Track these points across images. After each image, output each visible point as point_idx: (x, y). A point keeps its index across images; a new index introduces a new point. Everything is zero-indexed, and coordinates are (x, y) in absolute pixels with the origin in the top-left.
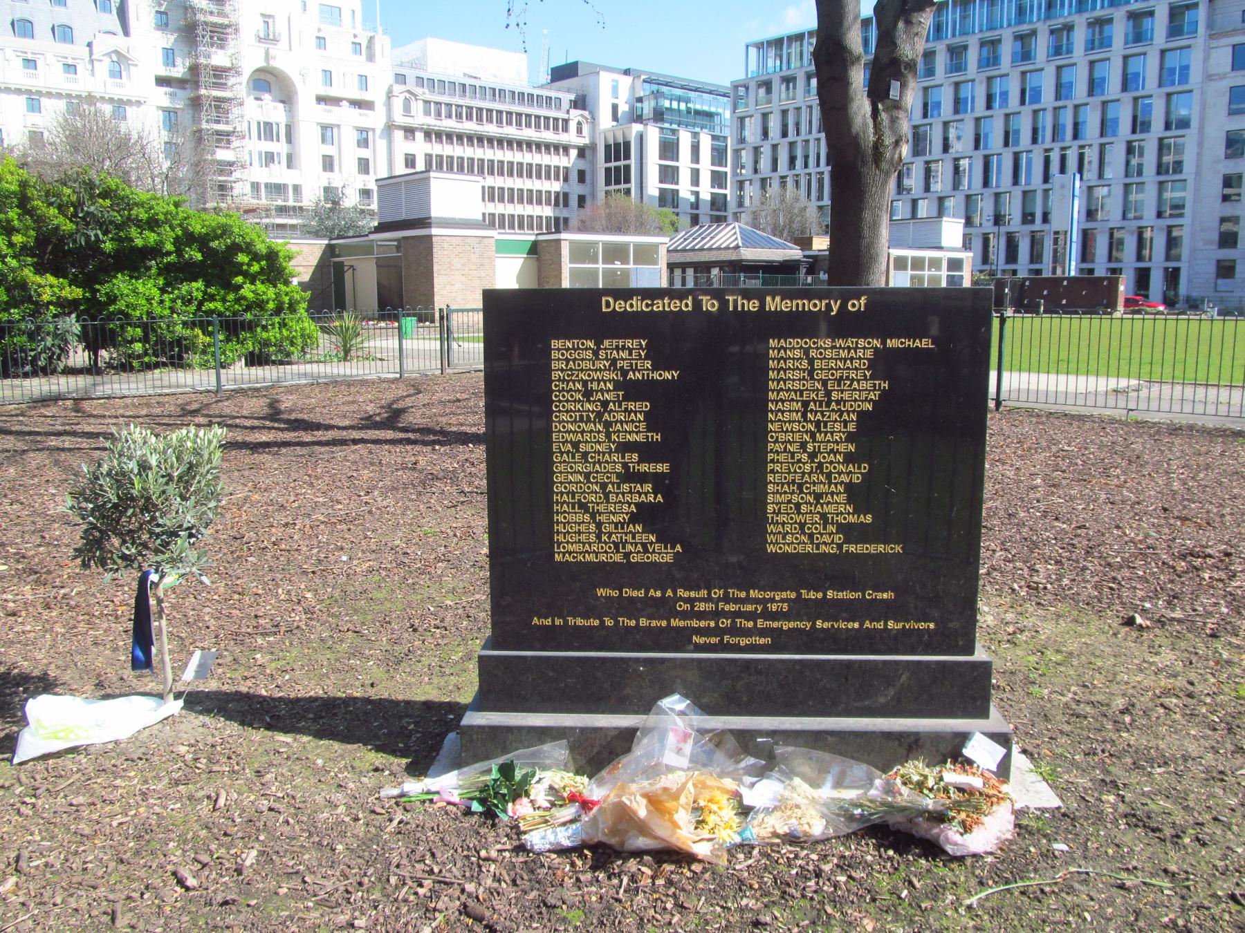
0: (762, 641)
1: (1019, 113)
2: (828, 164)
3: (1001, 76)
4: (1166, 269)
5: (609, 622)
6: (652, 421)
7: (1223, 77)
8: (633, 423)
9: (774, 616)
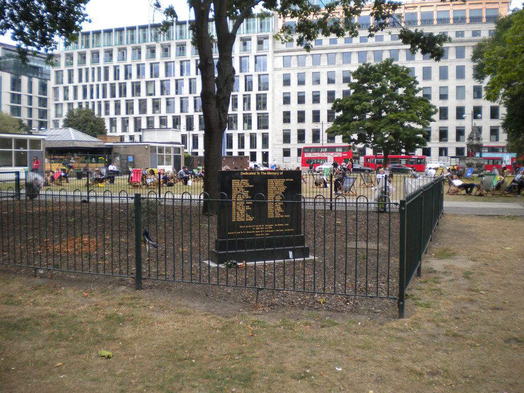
0: (267, 234)
1: (195, 79)
2: (201, 129)
3: (186, 61)
4: (263, 152)
5: (242, 232)
6: (249, 194)
7: (280, 69)
8: (246, 194)
9: (269, 230)
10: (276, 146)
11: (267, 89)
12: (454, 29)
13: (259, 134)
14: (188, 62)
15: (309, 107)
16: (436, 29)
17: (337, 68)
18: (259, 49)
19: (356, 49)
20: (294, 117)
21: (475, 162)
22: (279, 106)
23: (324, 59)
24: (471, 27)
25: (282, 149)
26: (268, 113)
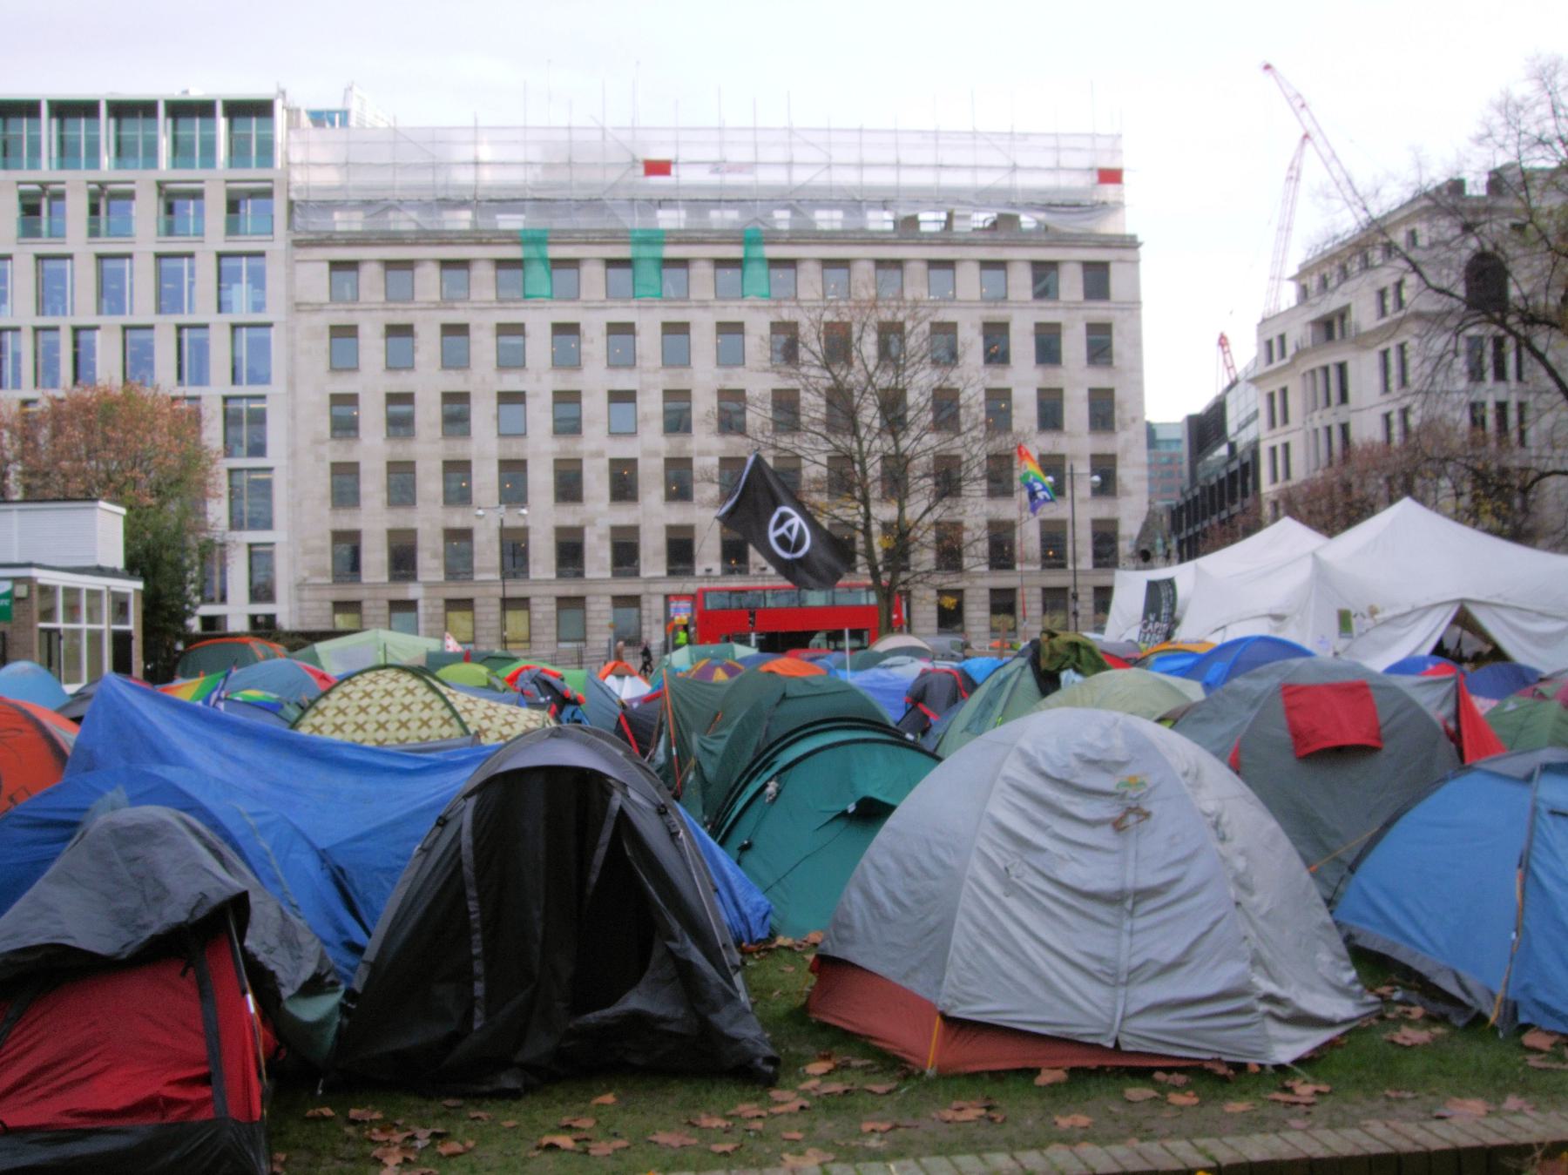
7: (318, 308)
11: (266, 380)
14: (256, 262)
18: (232, 229)
22: (318, 442)
26: (269, 470)
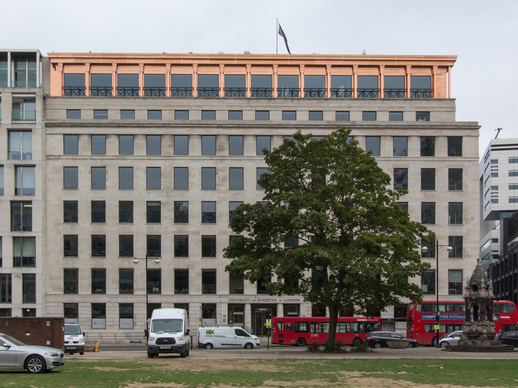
7: (58, 158)
10: (50, 299)
12: (360, 107)
13: (18, 276)
15: (195, 230)
16: (331, 105)
17: (163, 161)
19: (196, 129)
20: (85, 247)
21: (485, 331)
22: (57, 224)
23: (140, 145)
24: (387, 105)
25: (62, 305)
